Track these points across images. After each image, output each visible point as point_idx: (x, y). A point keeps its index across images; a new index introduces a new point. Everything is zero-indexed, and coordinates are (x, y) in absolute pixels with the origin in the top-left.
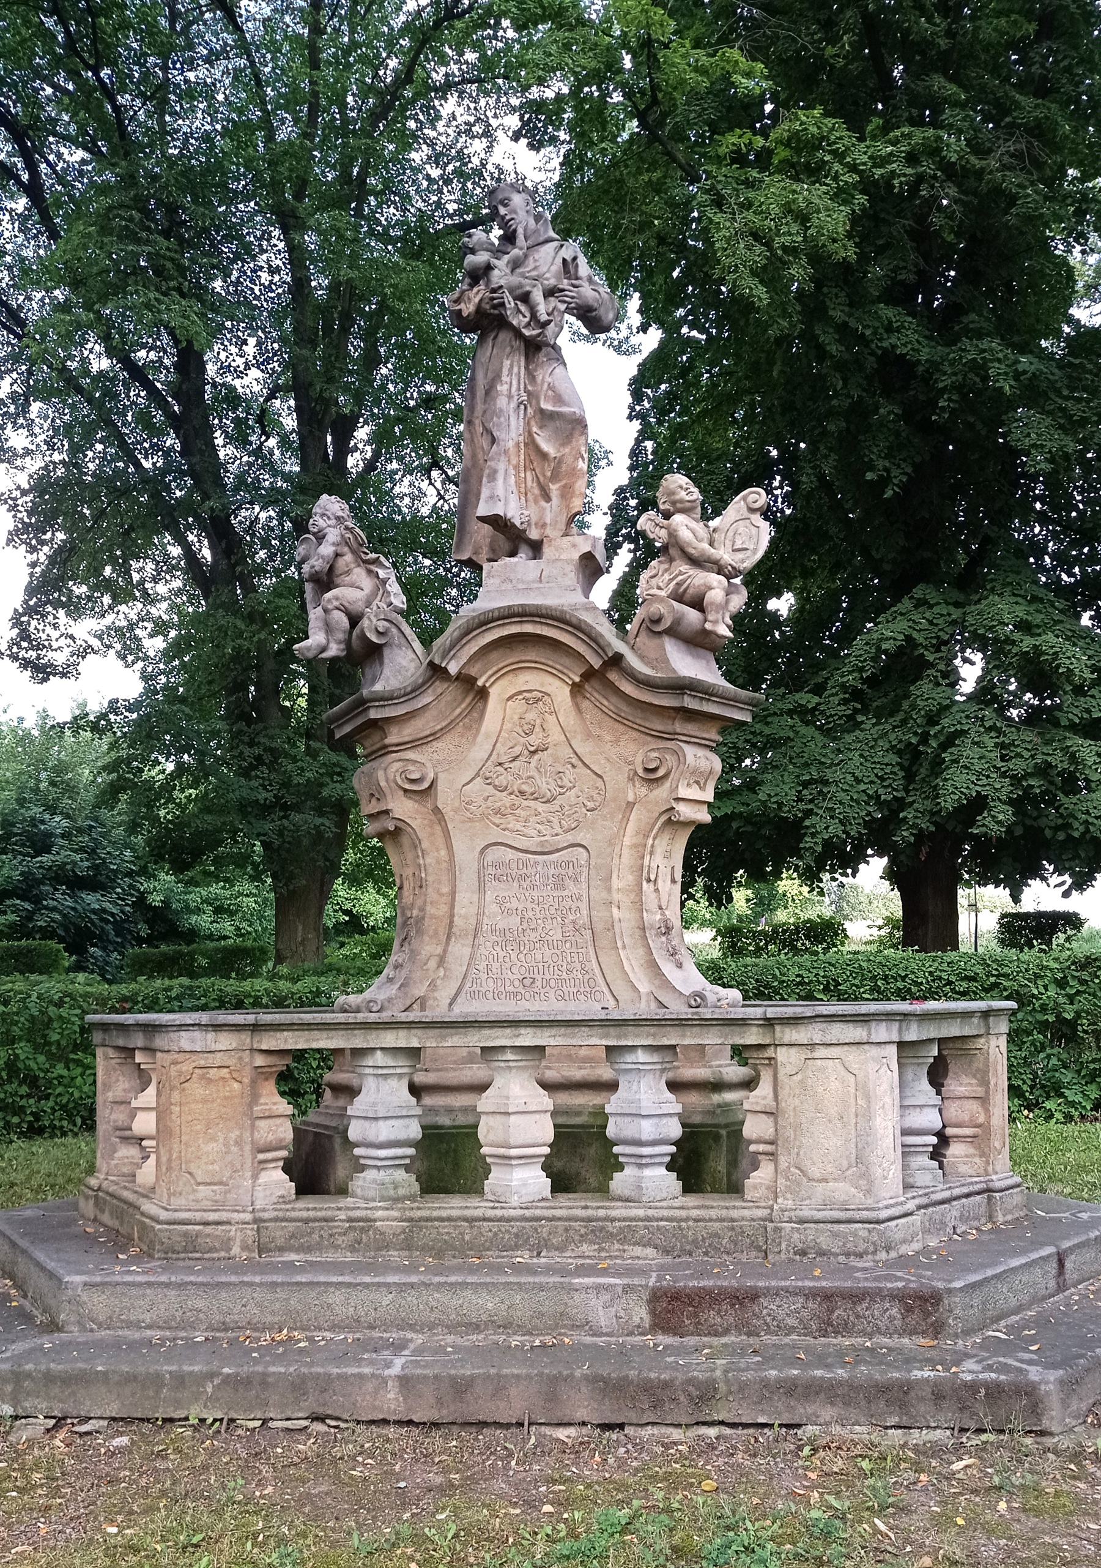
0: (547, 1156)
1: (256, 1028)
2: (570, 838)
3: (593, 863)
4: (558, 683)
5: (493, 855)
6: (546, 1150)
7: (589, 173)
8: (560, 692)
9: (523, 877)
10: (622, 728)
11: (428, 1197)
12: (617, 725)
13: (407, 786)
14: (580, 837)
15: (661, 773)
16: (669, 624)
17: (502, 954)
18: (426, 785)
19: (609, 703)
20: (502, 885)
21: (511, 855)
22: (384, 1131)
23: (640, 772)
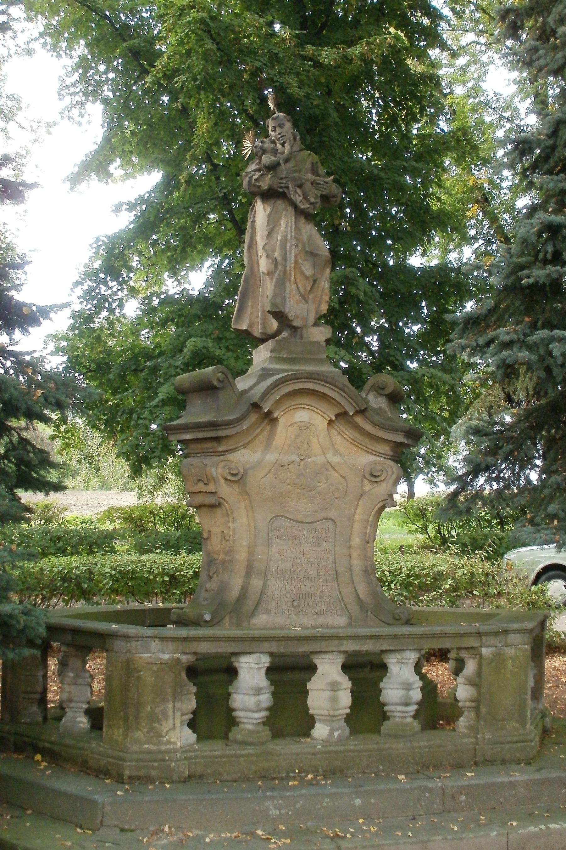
0: (347, 715)
1: (186, 639)
2: (324, 514)
3: (338, 530)
4: (320, 418)
5: (277, 523)
6: (348, 711)
7: (498, 181)
8: (320, 423)
9: (295, 537)
10: (355, 448)
11: (277, 741)
12: (352, 446)
13: (229, 478)
14: (332, 514)
15: (382, 478)
16: (390, 391)
17: (281, 585)
18: (239, 477)
19: (349, 432)
20: (282, 542)
21: (288, 524)
22: (251, 701)
23: (368, 476)
